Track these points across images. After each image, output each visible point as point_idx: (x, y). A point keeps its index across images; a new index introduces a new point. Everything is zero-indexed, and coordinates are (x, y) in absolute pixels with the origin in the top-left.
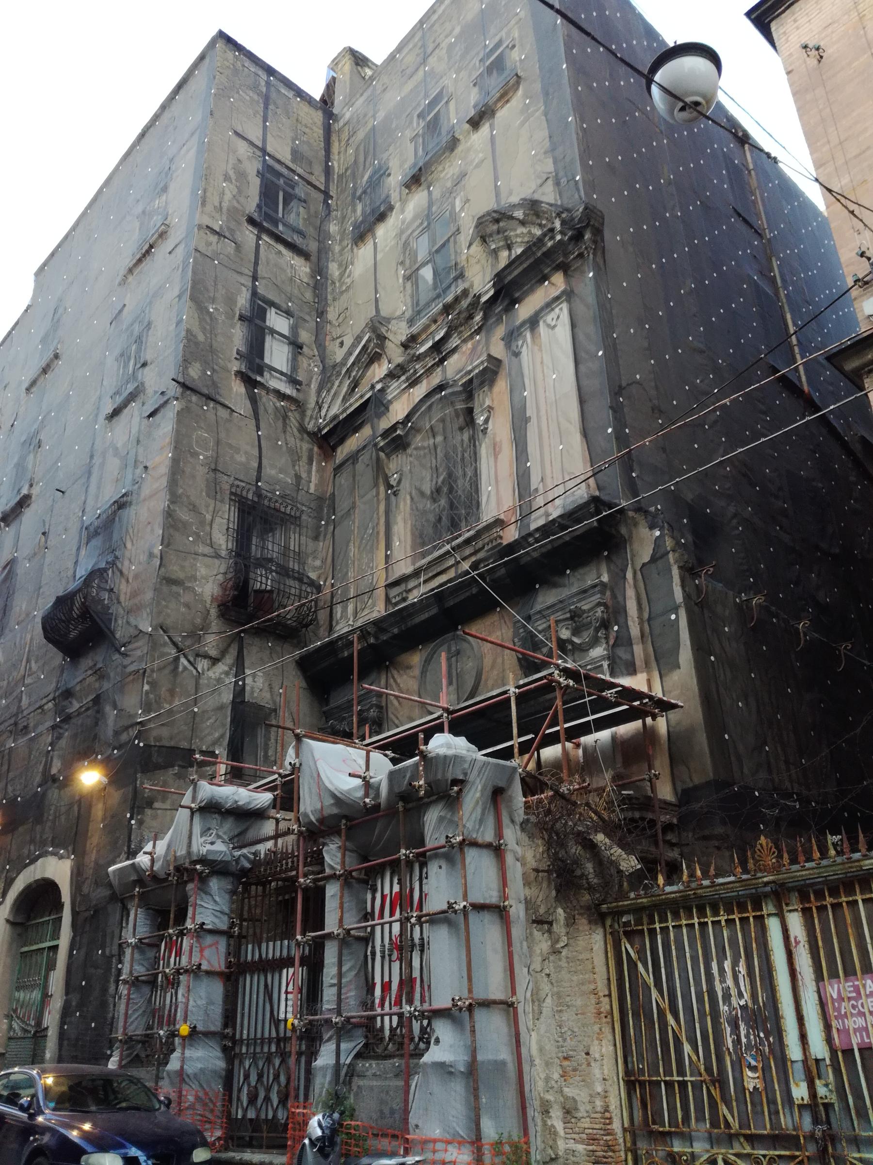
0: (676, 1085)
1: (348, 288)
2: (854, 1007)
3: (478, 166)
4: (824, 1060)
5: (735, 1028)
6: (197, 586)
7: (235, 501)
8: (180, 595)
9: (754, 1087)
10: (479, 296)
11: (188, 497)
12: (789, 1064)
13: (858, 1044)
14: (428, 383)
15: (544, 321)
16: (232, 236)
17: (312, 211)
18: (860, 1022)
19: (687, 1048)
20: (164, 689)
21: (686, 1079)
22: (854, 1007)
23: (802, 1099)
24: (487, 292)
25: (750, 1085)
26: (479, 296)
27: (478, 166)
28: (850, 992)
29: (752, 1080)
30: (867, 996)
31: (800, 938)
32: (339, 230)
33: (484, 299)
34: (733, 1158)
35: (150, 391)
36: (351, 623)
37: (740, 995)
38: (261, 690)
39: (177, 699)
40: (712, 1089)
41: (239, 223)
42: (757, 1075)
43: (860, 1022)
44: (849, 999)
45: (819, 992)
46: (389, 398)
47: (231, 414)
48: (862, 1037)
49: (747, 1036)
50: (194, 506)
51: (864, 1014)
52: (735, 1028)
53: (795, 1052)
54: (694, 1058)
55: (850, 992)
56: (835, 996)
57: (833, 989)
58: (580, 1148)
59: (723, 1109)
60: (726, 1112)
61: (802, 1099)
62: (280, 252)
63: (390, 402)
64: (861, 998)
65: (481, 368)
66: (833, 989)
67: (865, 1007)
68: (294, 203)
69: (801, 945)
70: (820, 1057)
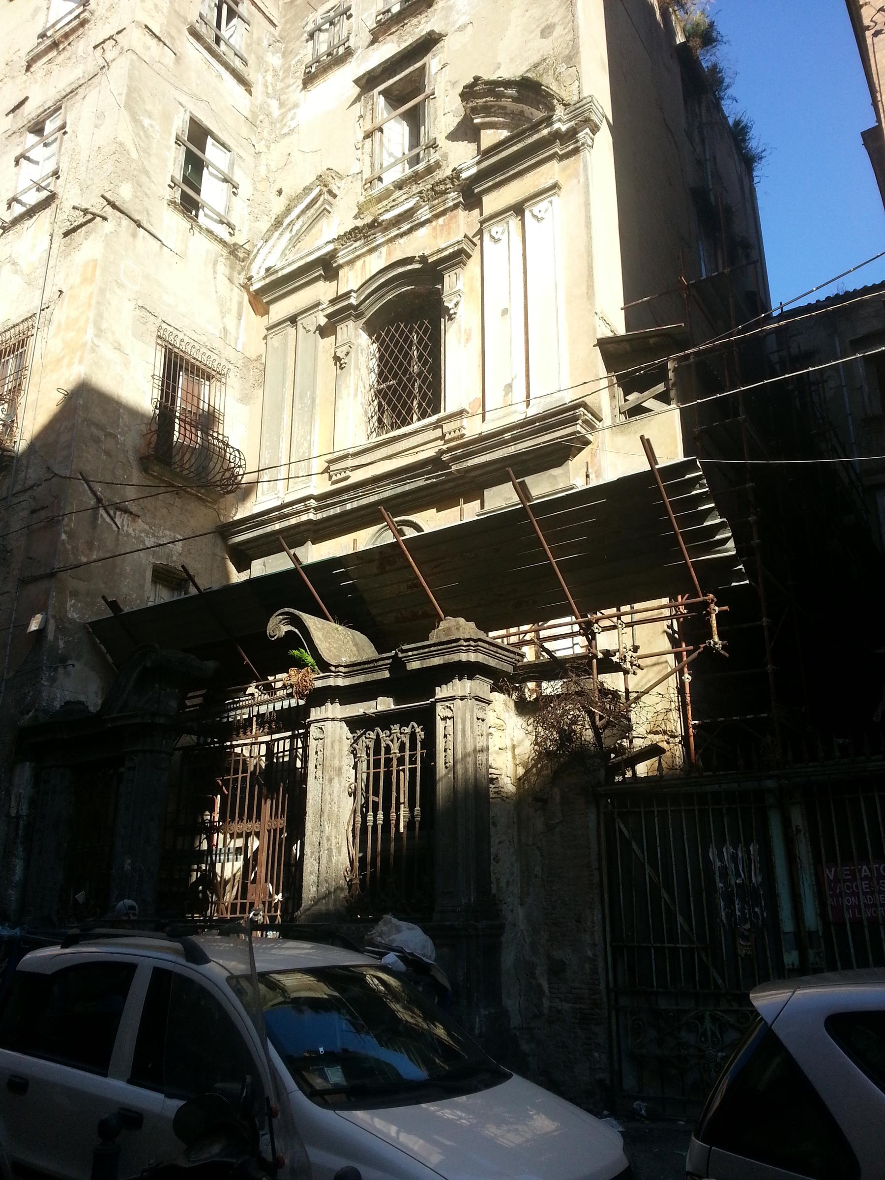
0: (681, 950)
1: (291, 132)
2: (848, 888)
3: (461, 29)
4: (817, 932)
5: (730, 903)
6: (119, 433)
7: (161, 345)
8: (101, 441)
9: (746, 953)
10: (461, 171)
11: (113, 333)
12: (782, 934)
13: (849, 919)
14: (389, 253)
15: (531, 211)
16: (172, 44)
17: (255, 36)
18: (854, 900)
19: (680, 919)
20: (81, 541)
21: (678, 945)
22: (848, 888)
23: (793, 964)
24: (468, 168)
25: (742, 952)
26: (461, 171)
27: (461, 29)
28: (846, 875)
29: (744, 948)
30: (862, 879)
31: (801, 827)
32: (284, 65)
33: (464, 175)
34: (721, 1014)
35: (67, 206)
36: (281, 495)
37: (738, 875)
38: (180, 554)
39: (95, 553)
40: (703, 955)
41: (180, 31)
42: (749, 944)
43: (854, 900)
44: (845, 881)
45: (816, 875)
46: (341, 262)
47: (161, 248)
48: (853, 912)
49: (742, 910)
50: (120, 345)
51: (858, 895)
52: (730, 903)
53: (787, 925)
54: (686, 928)
55: (846, 875)
56: (832, 878)
57: (830, 871)
58: (566, 1006)
59: (714, 973)
60: (716, 975)
61: (793, 964)
62: (220, 76)
63: (340, 266)
64: (856, 881)
65: (456, 248)
66: (830, 871)
67: (860, 888)
68: (235, 21)
69: (802, 833)
70: (813, 929)
